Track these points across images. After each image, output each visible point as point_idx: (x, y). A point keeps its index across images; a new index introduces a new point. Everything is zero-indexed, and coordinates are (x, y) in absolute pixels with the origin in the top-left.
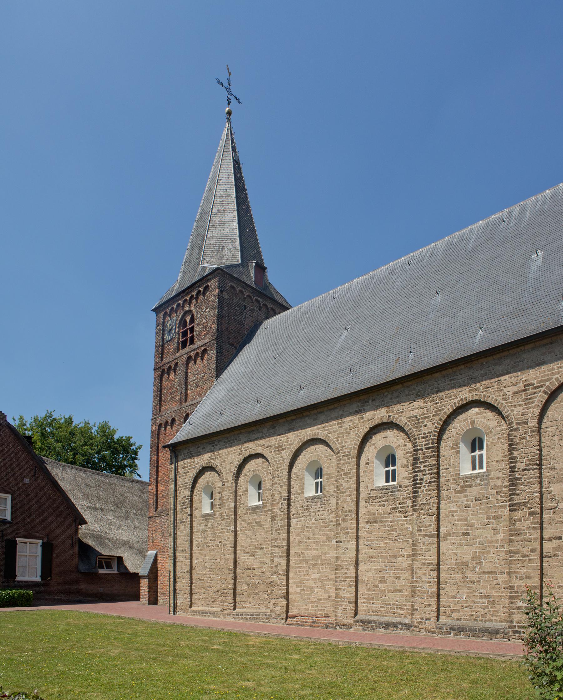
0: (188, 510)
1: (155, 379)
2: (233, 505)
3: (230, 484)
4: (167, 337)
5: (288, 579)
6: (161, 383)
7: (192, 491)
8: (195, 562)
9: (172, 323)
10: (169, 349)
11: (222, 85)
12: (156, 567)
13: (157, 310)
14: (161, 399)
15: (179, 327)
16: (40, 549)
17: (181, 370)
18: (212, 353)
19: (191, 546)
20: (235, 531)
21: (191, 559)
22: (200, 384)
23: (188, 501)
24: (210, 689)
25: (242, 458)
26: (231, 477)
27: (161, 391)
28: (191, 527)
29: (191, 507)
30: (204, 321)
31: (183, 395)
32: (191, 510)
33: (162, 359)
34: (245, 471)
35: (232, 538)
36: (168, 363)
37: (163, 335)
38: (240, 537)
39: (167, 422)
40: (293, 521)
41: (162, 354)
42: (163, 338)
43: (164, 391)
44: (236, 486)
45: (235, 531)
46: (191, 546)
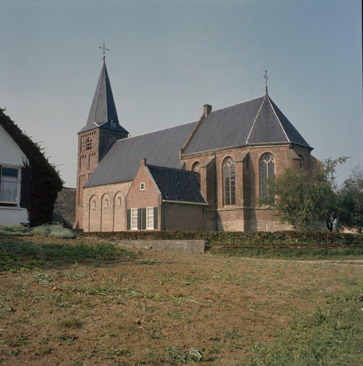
0: (89, 207)
1: (78, 159)
2: (101, 207)
3: (100, 201)
4: (83, 145)
5: (113, 227)
6: (80, 161)
7: (90, 202)
8: (90, 223)
9: (85, 139)
10: (83, 149)
11: (107, 50)
12: (78, 225)
13: (79, 134)
14: (80, 166)
15: (87, 142)
16: (19, 186)
17: (88, 158)
18: (97, 154)
19: (89, 218)
20: (101, 214)
21: (89, 222)
22: (94, 163)
23: (88, 205)
24: (113, 248)
25: (103, 194)
26: (100, 199)
27: (80, 163)
28: (89, 212)
29: (89, 206)
30: (95, 142)
31: (88, 166)
32: (89, 207)
33: (81, 152)
34: (103, 198)
35: (100, 216)
36: (83, 154)
37: (81, 143)
38: (103, 216)
39: (82, 175)
40: (115, 212)
41: (81, 150)
42: (81, 145)
43: (82, 164)
44: (102, 202)
45: (101, 214)
46: (89, 218)
